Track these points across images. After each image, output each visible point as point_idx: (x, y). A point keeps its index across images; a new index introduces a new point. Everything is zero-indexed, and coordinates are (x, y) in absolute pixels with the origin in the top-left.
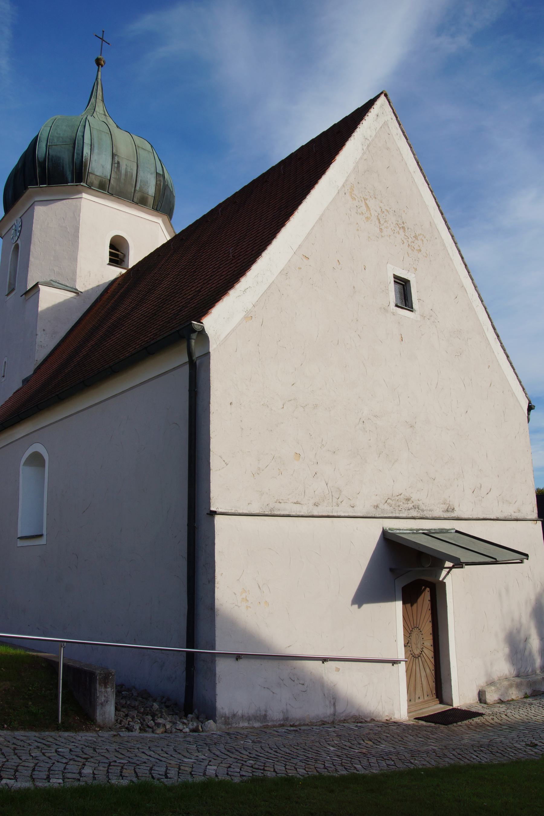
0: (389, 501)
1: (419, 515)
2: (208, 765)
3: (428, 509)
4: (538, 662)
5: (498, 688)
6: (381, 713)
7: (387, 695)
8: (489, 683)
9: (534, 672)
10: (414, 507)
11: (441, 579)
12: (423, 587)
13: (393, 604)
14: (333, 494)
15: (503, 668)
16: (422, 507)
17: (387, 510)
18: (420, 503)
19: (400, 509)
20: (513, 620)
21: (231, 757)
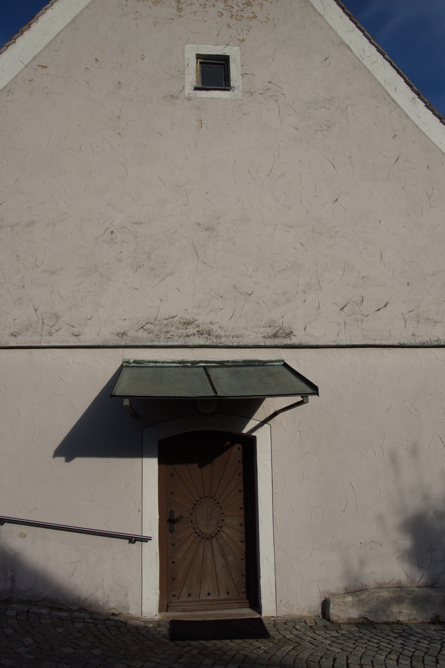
0: (148, 326)
3: (232, 334)
5: (360, 601)
6: (101, 603)
7: (134, 586)
10: (201, 333)
11: (245, 431)
12: (228, 443)
13: (137, 461)
14: (45, 321)
17: (143, 337)
20: (426, 498)
21: (311, 637)
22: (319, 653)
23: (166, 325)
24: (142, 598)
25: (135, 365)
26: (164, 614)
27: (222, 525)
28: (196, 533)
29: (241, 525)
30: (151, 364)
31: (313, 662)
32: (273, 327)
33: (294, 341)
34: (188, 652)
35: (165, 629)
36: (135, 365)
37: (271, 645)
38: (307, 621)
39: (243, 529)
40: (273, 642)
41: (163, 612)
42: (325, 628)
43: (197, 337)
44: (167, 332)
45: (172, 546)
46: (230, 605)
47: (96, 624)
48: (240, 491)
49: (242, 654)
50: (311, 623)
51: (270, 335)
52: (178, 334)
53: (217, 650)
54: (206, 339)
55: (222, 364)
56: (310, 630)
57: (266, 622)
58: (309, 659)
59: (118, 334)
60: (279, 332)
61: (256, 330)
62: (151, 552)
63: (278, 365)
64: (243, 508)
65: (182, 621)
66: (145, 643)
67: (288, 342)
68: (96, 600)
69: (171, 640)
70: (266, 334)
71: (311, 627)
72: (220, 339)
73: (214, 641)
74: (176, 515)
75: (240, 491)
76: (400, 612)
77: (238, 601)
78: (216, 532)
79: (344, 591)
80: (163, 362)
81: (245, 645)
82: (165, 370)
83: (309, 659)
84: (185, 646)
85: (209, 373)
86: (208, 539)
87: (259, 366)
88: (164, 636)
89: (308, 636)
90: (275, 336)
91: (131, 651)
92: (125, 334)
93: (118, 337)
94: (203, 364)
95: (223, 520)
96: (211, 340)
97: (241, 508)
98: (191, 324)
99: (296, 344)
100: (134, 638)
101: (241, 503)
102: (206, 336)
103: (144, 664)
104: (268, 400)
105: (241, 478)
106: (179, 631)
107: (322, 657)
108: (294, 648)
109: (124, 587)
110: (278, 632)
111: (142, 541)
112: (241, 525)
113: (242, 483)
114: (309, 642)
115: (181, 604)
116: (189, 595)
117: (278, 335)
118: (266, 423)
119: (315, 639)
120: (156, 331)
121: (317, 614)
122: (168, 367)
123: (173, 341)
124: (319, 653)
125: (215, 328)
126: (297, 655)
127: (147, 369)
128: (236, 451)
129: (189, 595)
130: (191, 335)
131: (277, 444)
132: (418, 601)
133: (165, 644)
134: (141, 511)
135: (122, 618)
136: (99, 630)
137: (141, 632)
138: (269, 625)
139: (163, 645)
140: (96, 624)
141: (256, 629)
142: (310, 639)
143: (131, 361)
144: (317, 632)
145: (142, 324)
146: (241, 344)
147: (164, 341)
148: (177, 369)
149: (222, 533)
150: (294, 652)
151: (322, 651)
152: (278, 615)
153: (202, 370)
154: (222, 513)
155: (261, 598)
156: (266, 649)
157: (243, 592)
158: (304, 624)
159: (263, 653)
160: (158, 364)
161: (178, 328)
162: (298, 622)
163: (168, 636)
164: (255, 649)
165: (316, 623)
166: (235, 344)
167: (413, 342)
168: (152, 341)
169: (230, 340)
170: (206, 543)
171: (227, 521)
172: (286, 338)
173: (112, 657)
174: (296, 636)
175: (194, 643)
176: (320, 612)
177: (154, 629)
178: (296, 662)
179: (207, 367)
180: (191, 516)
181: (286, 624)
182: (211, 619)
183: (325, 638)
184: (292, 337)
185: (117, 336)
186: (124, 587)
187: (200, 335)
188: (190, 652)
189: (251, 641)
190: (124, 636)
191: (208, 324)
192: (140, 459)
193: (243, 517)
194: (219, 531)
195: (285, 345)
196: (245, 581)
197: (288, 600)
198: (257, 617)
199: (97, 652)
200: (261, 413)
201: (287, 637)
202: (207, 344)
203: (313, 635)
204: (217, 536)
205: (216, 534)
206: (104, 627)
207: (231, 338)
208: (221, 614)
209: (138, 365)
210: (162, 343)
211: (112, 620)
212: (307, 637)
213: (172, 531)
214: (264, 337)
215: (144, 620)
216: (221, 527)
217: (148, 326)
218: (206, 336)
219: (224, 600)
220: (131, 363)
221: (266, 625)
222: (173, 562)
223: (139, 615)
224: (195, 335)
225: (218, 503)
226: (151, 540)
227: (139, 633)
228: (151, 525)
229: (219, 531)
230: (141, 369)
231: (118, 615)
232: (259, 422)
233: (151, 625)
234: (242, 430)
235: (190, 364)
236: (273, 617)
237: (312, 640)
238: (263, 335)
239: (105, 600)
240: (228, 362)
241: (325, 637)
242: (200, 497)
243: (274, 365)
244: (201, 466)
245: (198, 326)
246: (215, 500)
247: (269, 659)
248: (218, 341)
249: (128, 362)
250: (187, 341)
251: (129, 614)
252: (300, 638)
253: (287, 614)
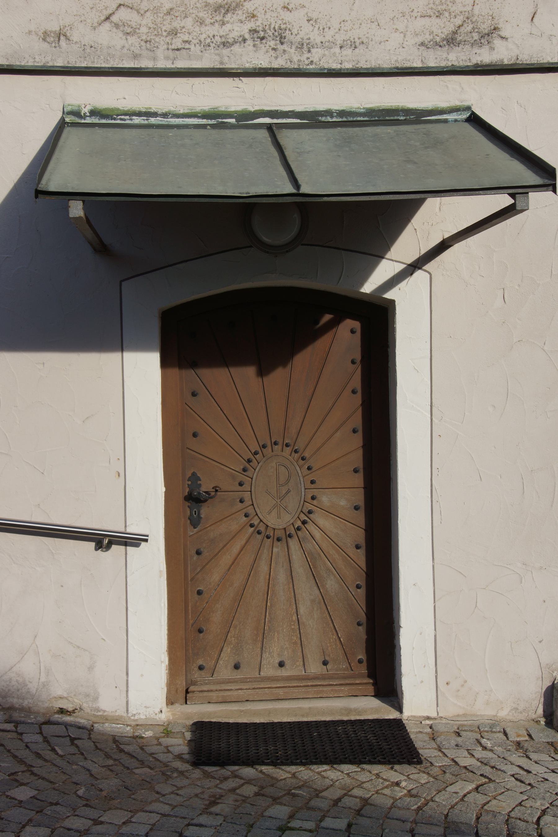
0: (123, 15)
6: (33, 687)
10: (258, 36)
11: (368, 288)
12: (327, 317)
13: (108, 360)
17: (112, 46)
22: (538, 803)
23: (168, 13)
24: (127, 674)
25: (95, 120)
26: (180, 709)
27: (311, 507)
28: (252, 526)
29: (356, 508)
30: (137, 120)
31: (524, 821)
32: (447, 14)
33: (502, 53)
34: (233, 790)
35: (180, 741)
36: (95, 120)
37: (424, 778)
38: (508, 730)
39: (360, 517)
40: (428, 774)
41: (177, 705)
42: (552, 750)
43: (251, 48)
44: (174, 33)
45: (196, 557)
46: (330, 688)
47: (22, 734)
48: (355, 431)
49: (356, 797)
50: (519, 736)
51: (438, 39)
52: (202, 37)
53: (300, 788)
54: (272, 53)
55: (313, 120)
56: (517, 750)
57: (412, 729)
58: (513, 814)
59: (45, 36)
60: (462, 29)
61: (401, 26)
62: (148, 569)
63: (456, 121)
64: (362, 470)
65: (220, 723)
66: (135, 771)
67: (485, 57)
68: (21, 680)
69: (196, 764)
70: (428, 37)
71: (518, 744)
72: (309, 51)
73: (294, 767)
74: (206, 486)
75: (355, 431)
77: (347, 681)
78: (299, 523)
80: (165, 115)
81: (363, 777)
82: (171, 133)
83: (513, 814)
84: (226, 779)
85: (282, 142)
86: (279, 540)
87: (405, 122)
88: (179, 757)
89: (512, 764)
90: (451, 41)
91: (101, 790)
92: (65, 35)
93: (46, 45)
94: (267, 120)
95: (313, 498)
96: (286, 56)
97: (356, 471)
98: (234, 9)
99: (506, 62)
100: (111, 762)
101: (357, 458)
102: (272, 43)
103: (132, 817)
104: (432, 204)
105: (358, 399)
106: (214, 745)
107: (544, 812)
108: (477, 789)
109: (85, 650)
110: (440, 750)
111: (126, 544)
112: (356, 508)
113: (360, 411)
114: (513, 776)
115: (218, 687)
116: (237, 667)
117: (459, 38)
118: (420, 268)
119: (529, 772)
120: (144, 30)
121: (534, 716)
122: (178, 127)
123: (190, 58)
124: (538, 803)
125: (296, 20)
126: (485, 804)
127: (126, 131)
128: (346, 337)
129: (237, 667)
130: (235, 42)
131: (453, 316)
133: (182, 773)
134: (122, 475)
135: (82, 718)
136: (27, 746)
137: (127, 748)
138: (420, 736)
139: (175, 775)
140: (22, 734)
141: (390, 743)
142: (517, 770)
143: (85, 110)
144: (533, 756)
145: (106, 8)
146: (363, 65)
147: (167, 58)
148: (202, 131)
149: (311, 526)
150: (478, 796)
151: (544, 799)
152: (440, 715)
153: (264, 134)
154: (313, 482)
155: (401, 674)
156: (411, 787)
157: (360, 661)
158: (501, 736)
159: (405, 795)
160: (153, 120)
161: (202, 22)
162: (487, 732)
163: (187, 757)
164: (387, 787)
165: (530, 736)
166: (348, 66)
168: (136, 57)
169: (334, 54)
170: (275, 550)
171: (325, 499)
172: (481, 45)
173: (57, 804)
174: (482, 762)
175: (248, 772)
176: (540, 711)
177: (155, 742)
178: (482, 819)
179: (275, 127)
180: (240, 488)
181: (458, 734)
182: (285, 720)
183: (553, 771)
184: (497, 42)
185: (44, 40)
186: (85, 650)
187: (258, 42)
188: (238, 791)
189: (376, 769)
190: (86, 759)
191: (279, 10)
192: (119, 354)
193: (362, 491)
194: (304, 522)
195: (477, 65)
196: (364, 637)
197: (466, 682)
198: (391, 717)
199: (23, 793)
200: (408, 244)
201: (462, 764)
202: (276, 65)
203: (523, 762)
204: (299, 533)
205: (299, 529)
206: (39, 738)
207: (337, 50)
208: (310, 708)
209: (104, 121)
210: (162, 64)
211: (57, 723)
212: (510, 766)
213: (195, 522)
214: (422, 44)
215: (134, 723)
216: (310, 512)
217: (123, 15)
218: (272, 43)
219: (316, 678)
220: (85, 117)
221: (412, 736)
222: (199, 593)
223: (121, 712)
224: (245, 40)
225: (303, 459)
226: (146, 540)
227: (122, 751)
228: (147, 507)
229: (304, 522)
230: (110, 132)
231: (74, 712)
232: (404, 266)
233: (149, 734)
234: (362, 284)
235: (233, 121)
236: (428, 718)
237: (522, 772)
238: (420, 39)
239: (43, 679)
240: (329, 113)
241: (552, 767)
242: (253, 451)
243: (446, 121)
244: (262, 373)
245: (254, 16)
246: (296, 452)
247: (420, 808)
248: (304, 58)
249: (77, 113)
250: (226, 59)
251: (98, 710)
252: (493, 767)
253: (461, 712)
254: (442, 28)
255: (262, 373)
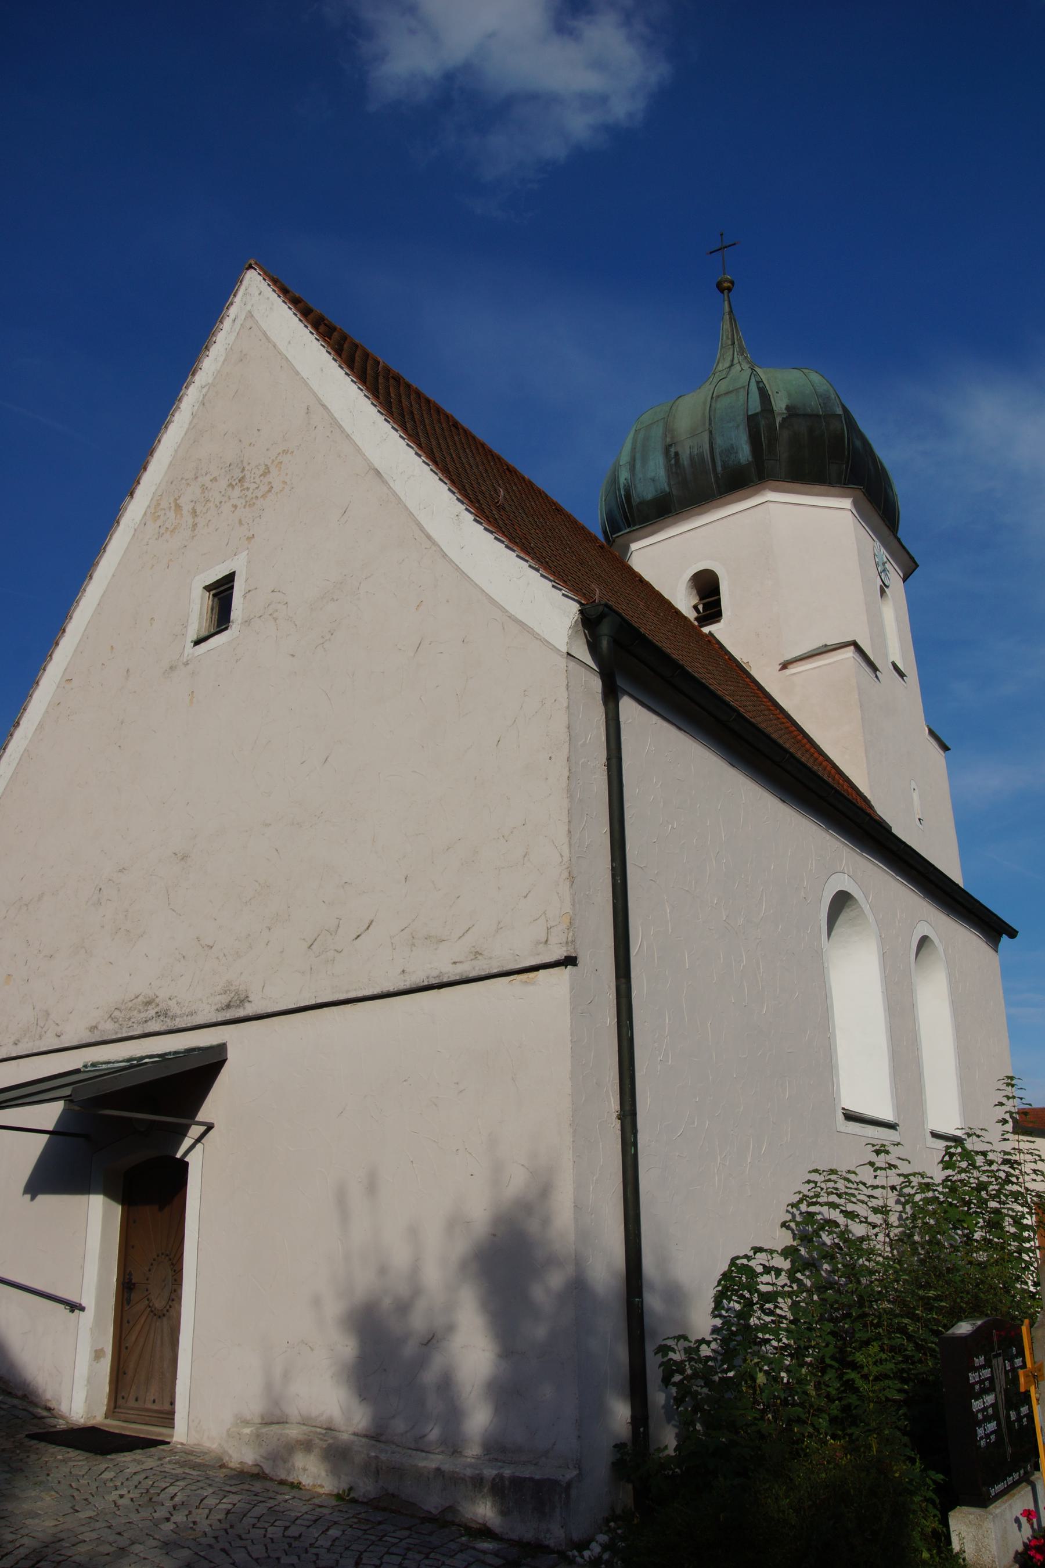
1: (164, 1028)
2: (387, 1553)
4: (479, 1419)
6: (40, 1391)
8: (266, 1420)
9: (453, 1445)
11: (178, 1155)
13: (83, 1198)
15: (325, 1397)
16: (175, 1010)
17: (109, 1029)
18: (172, 1004)
19: (130, 1024)
20: (383, 1270)
33: (249, 1010)
76: (305, 1470)
79: (260, 1421)
90: (228, 1006)
132: (336, 1454)
161: (139, 1012)
167: (401, 986)
184: (247, 1004)
254: (225, 999)
255: (1017, 1552)
